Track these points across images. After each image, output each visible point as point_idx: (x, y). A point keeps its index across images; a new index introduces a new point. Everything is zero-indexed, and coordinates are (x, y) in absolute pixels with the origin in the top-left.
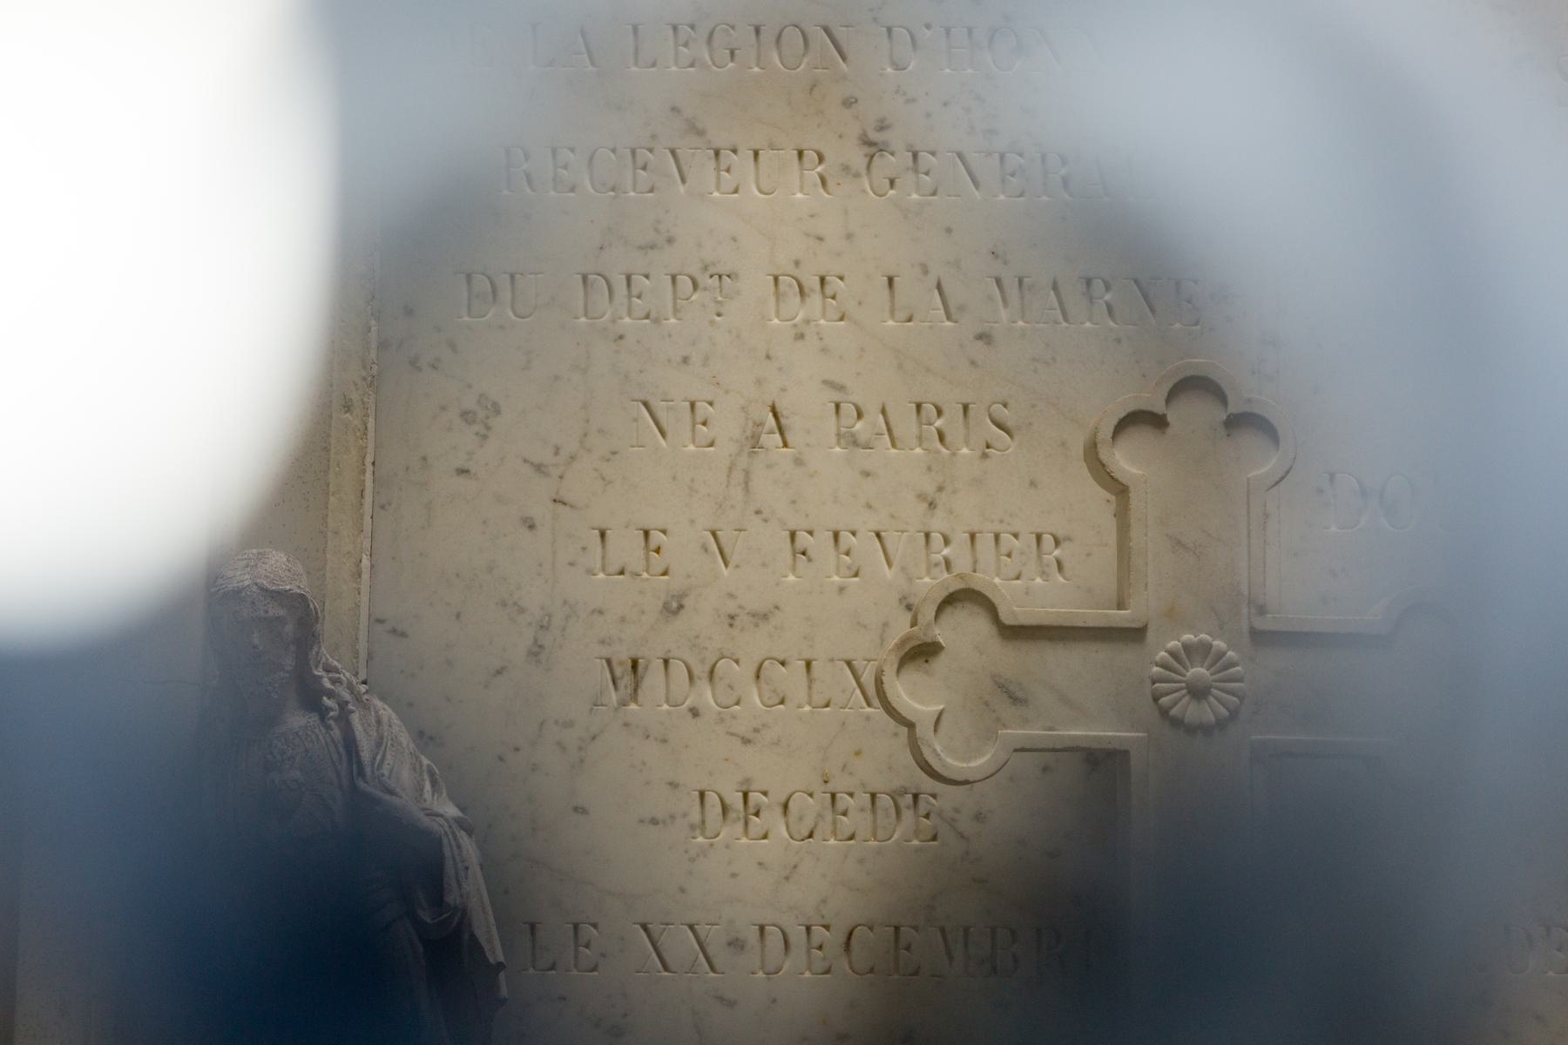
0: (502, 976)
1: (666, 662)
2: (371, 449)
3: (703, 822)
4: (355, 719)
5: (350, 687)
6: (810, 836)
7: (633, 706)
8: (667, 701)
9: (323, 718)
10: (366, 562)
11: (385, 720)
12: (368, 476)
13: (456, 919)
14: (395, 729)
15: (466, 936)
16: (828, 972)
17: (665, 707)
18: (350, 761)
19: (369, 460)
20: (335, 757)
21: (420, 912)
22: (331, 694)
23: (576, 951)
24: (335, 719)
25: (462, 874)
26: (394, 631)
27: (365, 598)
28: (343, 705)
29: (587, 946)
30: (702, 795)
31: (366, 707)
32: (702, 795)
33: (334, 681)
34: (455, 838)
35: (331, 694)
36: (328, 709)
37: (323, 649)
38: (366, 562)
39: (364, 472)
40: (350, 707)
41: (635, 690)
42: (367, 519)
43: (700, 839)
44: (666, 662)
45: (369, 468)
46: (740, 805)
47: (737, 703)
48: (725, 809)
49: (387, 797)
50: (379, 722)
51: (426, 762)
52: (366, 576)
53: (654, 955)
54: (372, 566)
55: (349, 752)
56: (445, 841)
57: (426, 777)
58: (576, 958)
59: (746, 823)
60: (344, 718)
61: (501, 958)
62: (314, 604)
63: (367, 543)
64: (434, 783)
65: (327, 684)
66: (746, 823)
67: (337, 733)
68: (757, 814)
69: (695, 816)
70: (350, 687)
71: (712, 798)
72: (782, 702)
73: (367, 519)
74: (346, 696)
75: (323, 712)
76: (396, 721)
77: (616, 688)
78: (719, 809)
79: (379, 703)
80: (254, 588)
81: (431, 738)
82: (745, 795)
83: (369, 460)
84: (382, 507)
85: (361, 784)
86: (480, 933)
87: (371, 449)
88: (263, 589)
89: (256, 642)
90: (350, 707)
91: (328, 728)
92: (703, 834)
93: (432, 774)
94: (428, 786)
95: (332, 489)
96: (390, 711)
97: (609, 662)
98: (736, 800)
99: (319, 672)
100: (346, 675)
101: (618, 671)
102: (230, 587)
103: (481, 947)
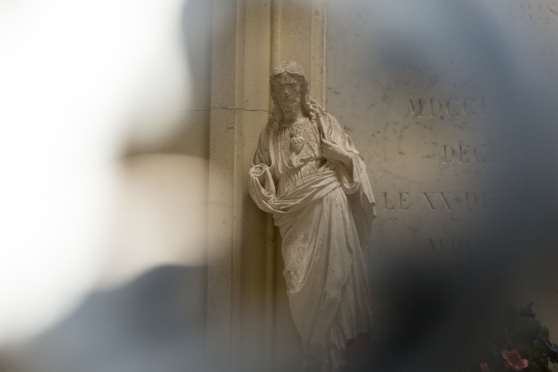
0: (374, 207)
1: (431, 100)
2: (325, 29)
3: (446, 157)
4: (321, 119)
5: (319, 108)
6: (484, 161)
7: (420, 116)
8: (432, 114)
9: (310, 119)
10: (324, 68)
11: (332, 120)
12: (325, 38)
13: (358, 187)
14: (336, 124)
15: (361, 193)
16: (468, 161)
17: (431, 116)
18: (320, 134)
19: (325, 32)
20: (315, 132)
21: (345, 185)
22: (313, 111)
23: (401, 202)
24: (315, 120)
25: (360, 171)
26: (335, 92)
27: (324, 80)
28: (317, 115)
29: (405, 201)
30: (445, 147)
31: (325, 116)
32: (445, 147)
33: (314, 107)
34: (357, 159)
35: (313, 111)
36: (312, 116)
37: (310, 96)
38: (324, 68)
39: (323, 37)
40: (320, 115)
41: (421, 111)
42: (325, 53)
43: (444, 163)
44: (431, 100)
45: (325, 35)
46: (459, 150)
47: (457, 115)
48: (453, 152)
49: (333, 144)
50: (330, 121)
51: (347, 135)
52: (325, 73)
53: (429, 204)
54: (327, 70)
55: (320, 131)
56: (353, 160)
57: (347, 140)
58: (401, 205)
59: (461, 157)
60: (318, 119)
61: (374, 201)
62: (307, 79)
63: (325, 62)
64: (349, 142)
65: (311, 107)
66: (461, 157)
67: (315, 124)
68: (465, 154)
69: (443, 154)
70: (319, 108)
71: (448, 148)
72: (473, 114)
73: (325, 53)
74: (318, 111)
75: (310, 118)
76: (336, 120)
77: (414, 110)
78: (451, 151)
79: (330, 115)
80: (286, 73)
81: (349, 129)
82: (461, 147)
83: (325, 32)
84: (330, 49)
85: (323, 140)
86: (366, 192)
87: (325, 29)
88: (289, 74)
89: (287, 92)
90: (320, 115)
91: (312, 122)
92: (445, 161)
93: (349, 139)
94: (347, 143)
95: (312, 42)
96: (333, 117)
97: (411, 101)
98: (457, 148)
99: (309, 103)
100: (318, 105)
101: (414, 104)
102: (277, 73)
103: (367, 197)
